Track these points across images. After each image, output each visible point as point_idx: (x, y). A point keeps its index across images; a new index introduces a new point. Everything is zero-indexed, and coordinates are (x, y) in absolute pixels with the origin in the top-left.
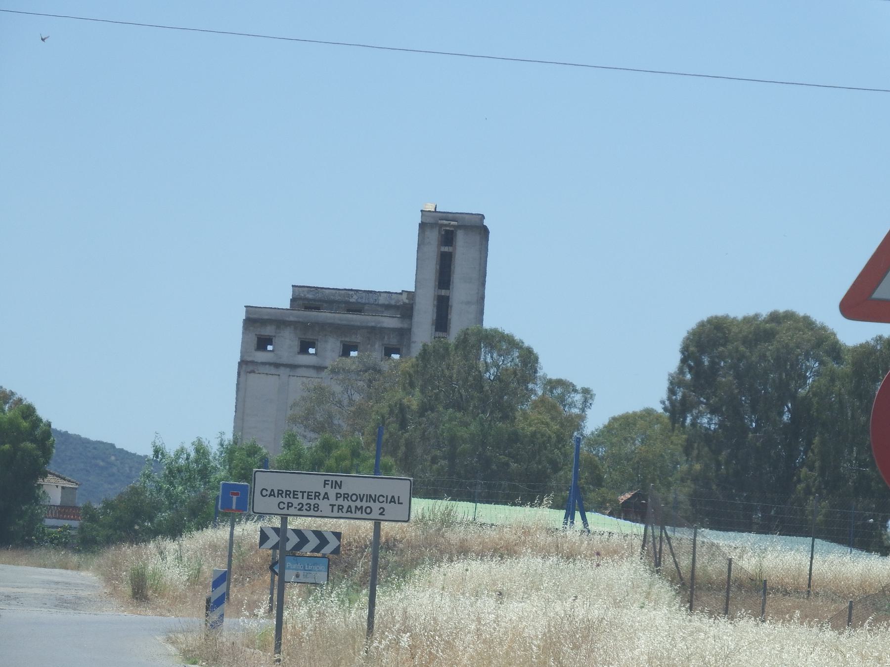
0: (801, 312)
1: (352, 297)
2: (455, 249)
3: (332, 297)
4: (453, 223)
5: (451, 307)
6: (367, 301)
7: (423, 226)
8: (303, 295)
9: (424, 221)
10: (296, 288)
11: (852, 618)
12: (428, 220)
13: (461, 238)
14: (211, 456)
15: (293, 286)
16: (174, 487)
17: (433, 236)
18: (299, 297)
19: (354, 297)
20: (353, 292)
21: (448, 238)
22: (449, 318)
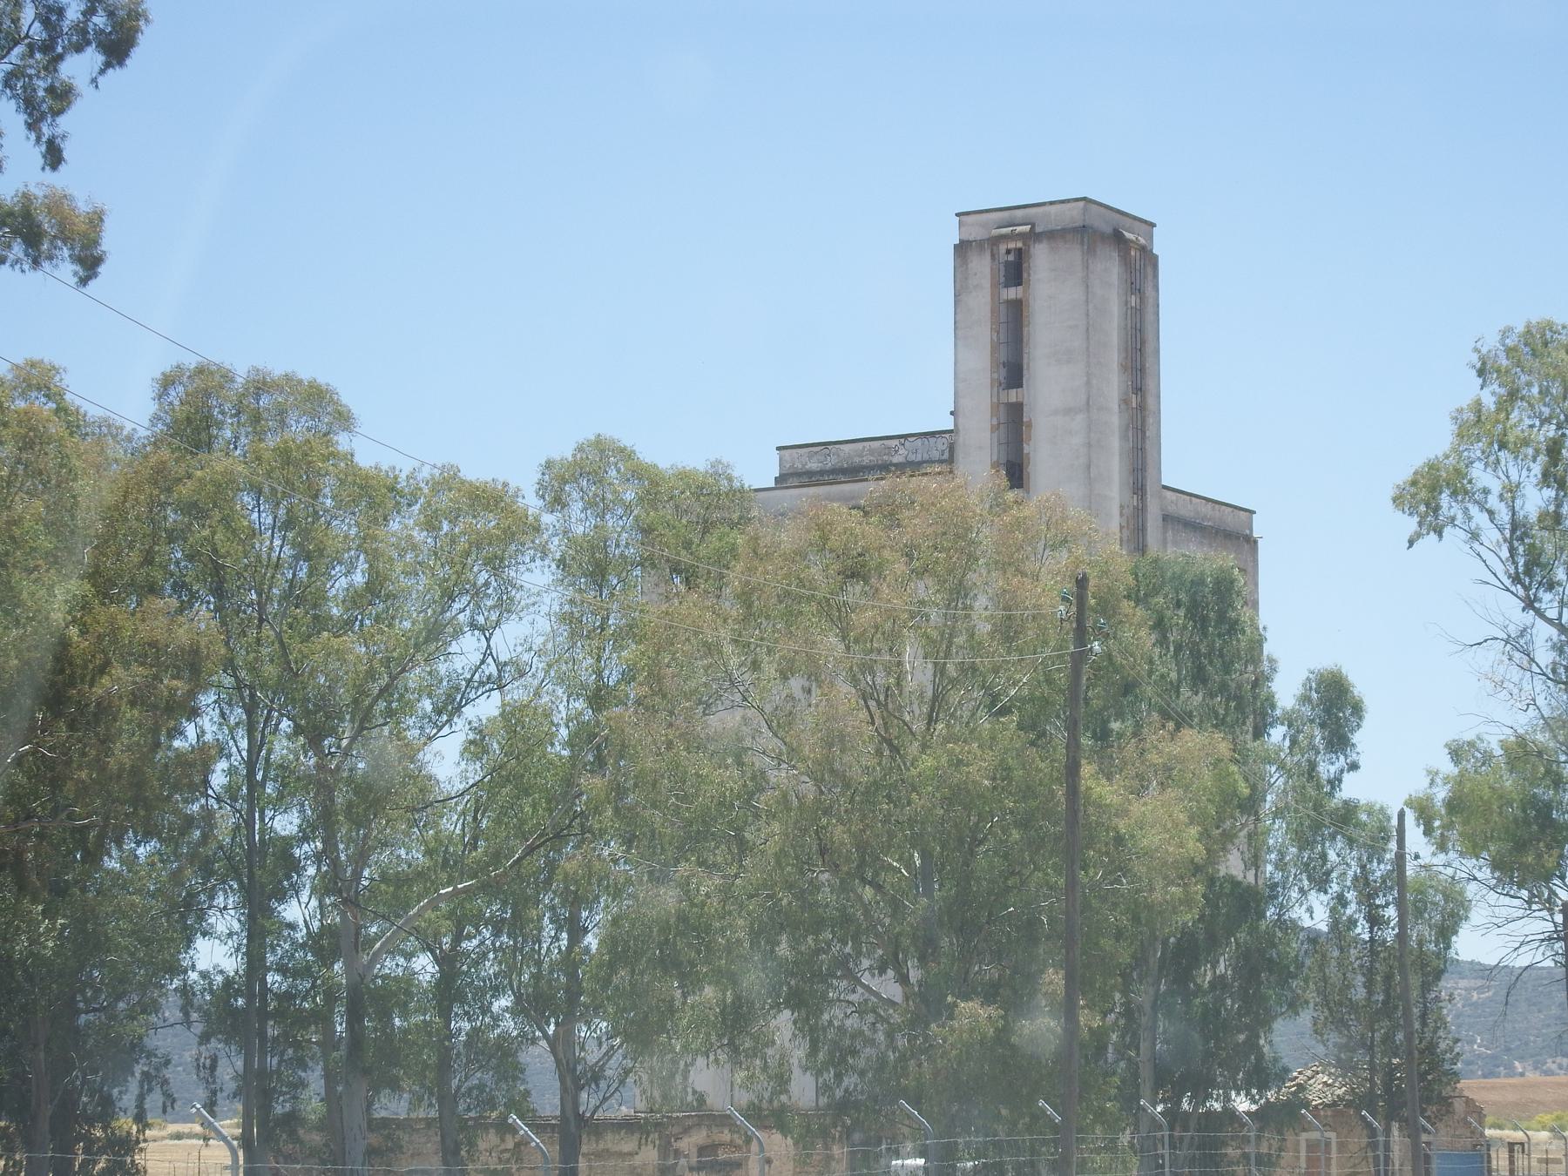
0: (305, 374)
1: (896, 451)
2: (995, 295)
3: (857, 460)
4: (1019, 229)
5: (1030, 425)
6: (926, 457)
7: (962, 249)
8: (800, 466)
9: (965, 237)
10: (787, 453)
11: (454, 648)
12: (975, 234)
13: (1042, 259)
14: (236, 760)
15: (779, 449)
16: (551, 985)
17: (982, 266)
18: (791, 471)
19: (901, 452)
20: (896, 442)
21: (1015, 272)
22: (1025, 451)
